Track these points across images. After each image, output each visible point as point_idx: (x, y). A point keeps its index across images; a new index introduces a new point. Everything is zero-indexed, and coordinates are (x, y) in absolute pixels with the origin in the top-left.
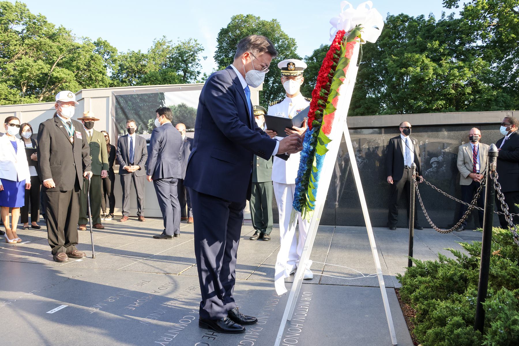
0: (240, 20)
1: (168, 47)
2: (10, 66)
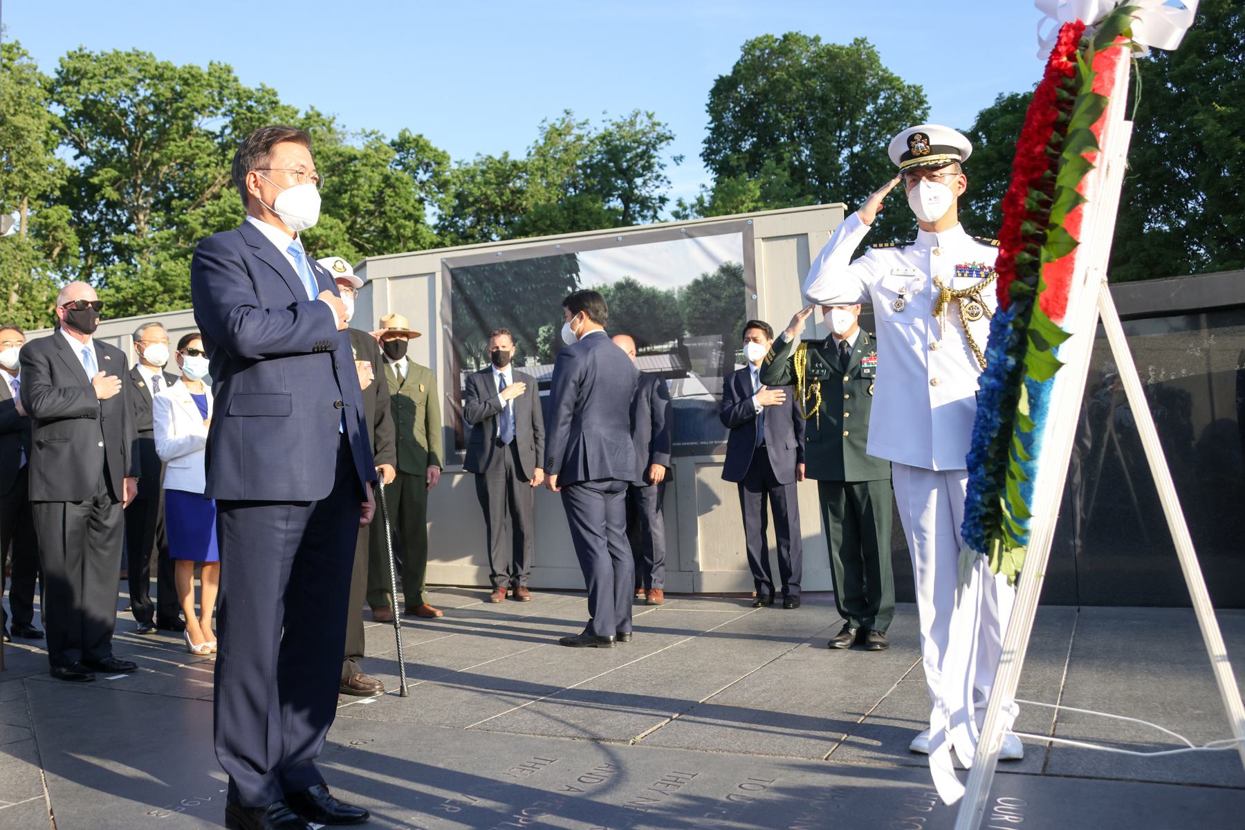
0: (767, 51)
1: (579, 138)
2: (194, 217)
